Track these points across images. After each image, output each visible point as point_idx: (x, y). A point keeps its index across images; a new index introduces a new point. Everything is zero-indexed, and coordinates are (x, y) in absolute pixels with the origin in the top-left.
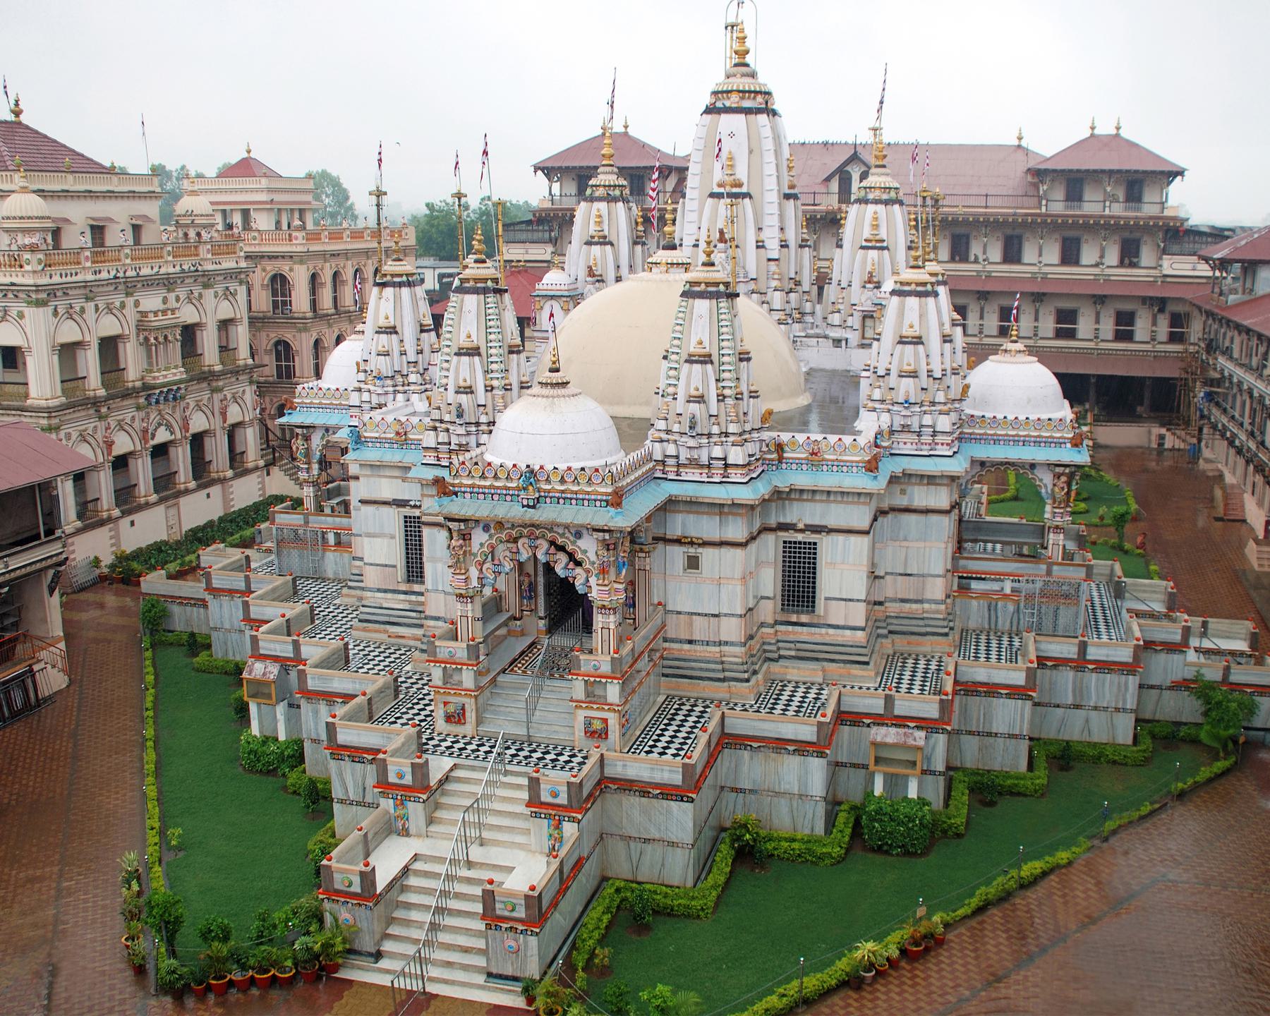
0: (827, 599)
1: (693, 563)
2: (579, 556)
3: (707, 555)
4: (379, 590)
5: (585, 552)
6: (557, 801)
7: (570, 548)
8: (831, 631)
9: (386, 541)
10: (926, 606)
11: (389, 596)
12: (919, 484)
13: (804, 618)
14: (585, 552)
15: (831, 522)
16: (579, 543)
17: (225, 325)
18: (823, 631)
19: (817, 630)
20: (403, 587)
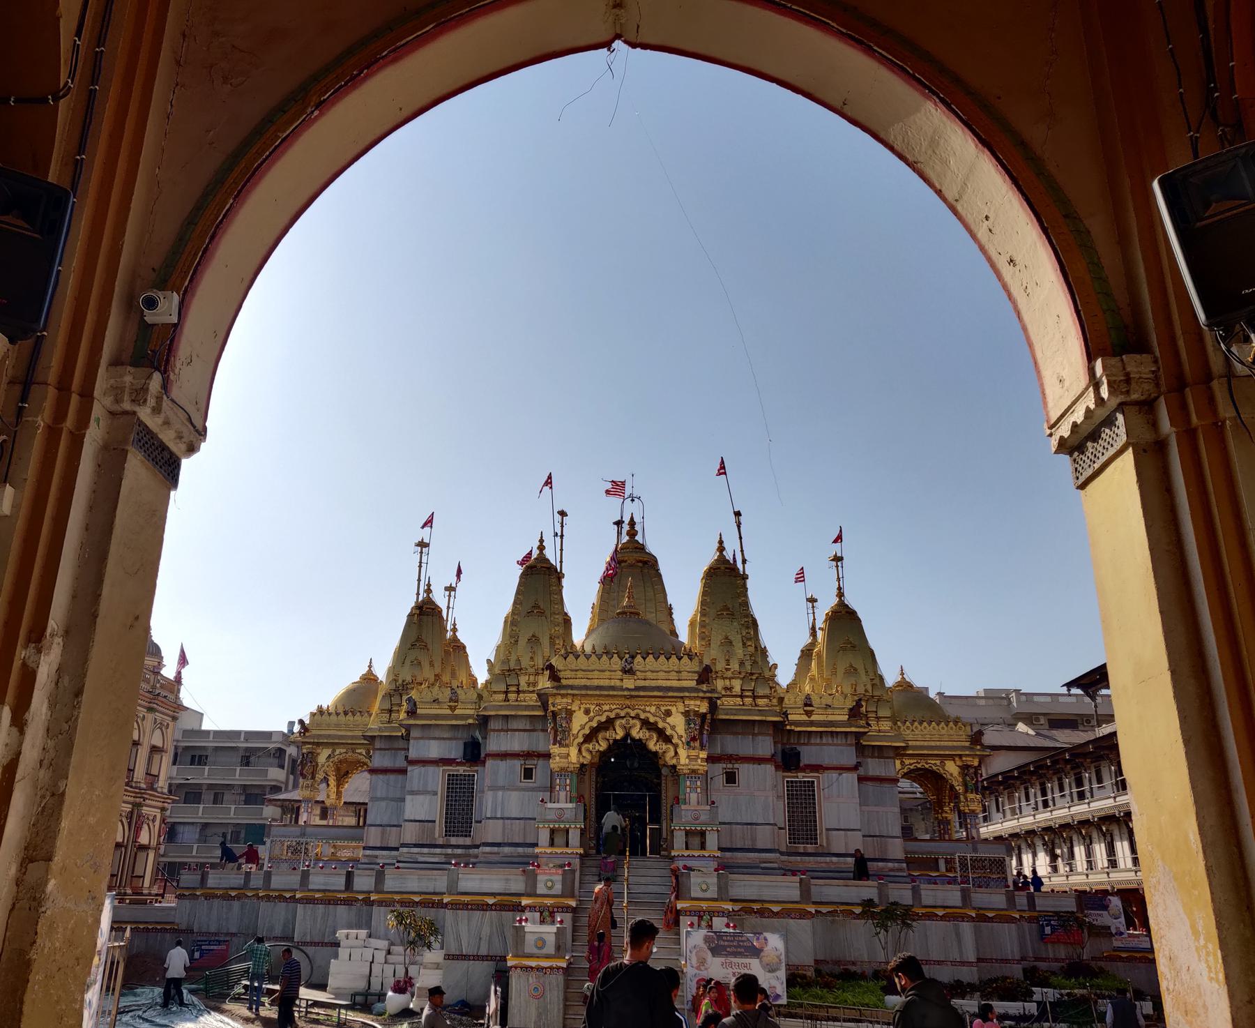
0: (827, 830)
1: (731, 778)
2: (669, 732)
3: (744, 770)
4: (416, 846)
5: (673, 728)
6: (708, 895)
7: (661, 725)
8: (835, 859)
9: (428, 797)
10: (890, 865)
11: (426, 850)
12: (873, 757)
13: (810, 848)
14: (673, 728)
15: (826, 762)
16: (669, 720)
17: (154, 749)
18: (828, 859)
19: (822, 859)
20: (440, 841)
